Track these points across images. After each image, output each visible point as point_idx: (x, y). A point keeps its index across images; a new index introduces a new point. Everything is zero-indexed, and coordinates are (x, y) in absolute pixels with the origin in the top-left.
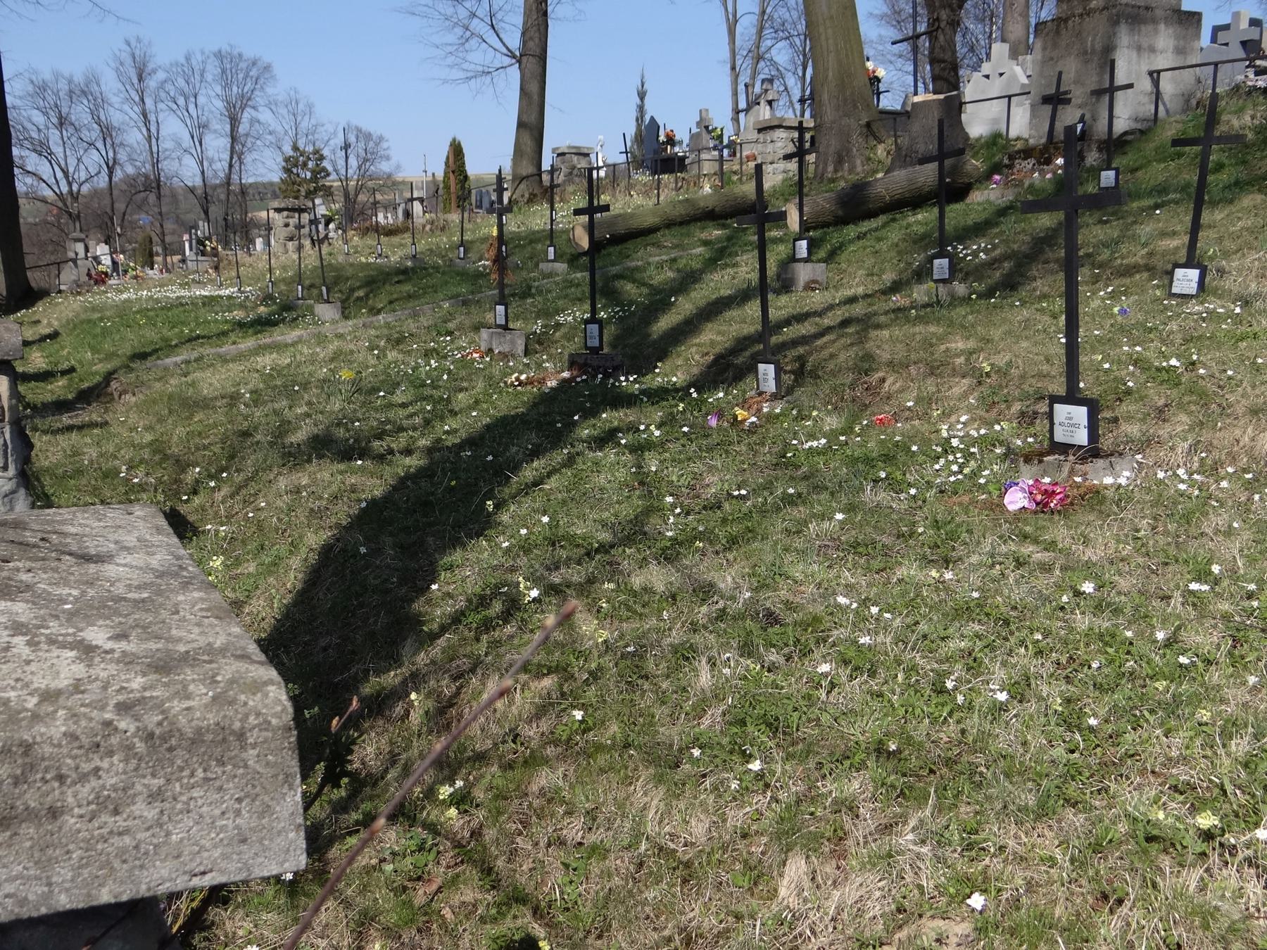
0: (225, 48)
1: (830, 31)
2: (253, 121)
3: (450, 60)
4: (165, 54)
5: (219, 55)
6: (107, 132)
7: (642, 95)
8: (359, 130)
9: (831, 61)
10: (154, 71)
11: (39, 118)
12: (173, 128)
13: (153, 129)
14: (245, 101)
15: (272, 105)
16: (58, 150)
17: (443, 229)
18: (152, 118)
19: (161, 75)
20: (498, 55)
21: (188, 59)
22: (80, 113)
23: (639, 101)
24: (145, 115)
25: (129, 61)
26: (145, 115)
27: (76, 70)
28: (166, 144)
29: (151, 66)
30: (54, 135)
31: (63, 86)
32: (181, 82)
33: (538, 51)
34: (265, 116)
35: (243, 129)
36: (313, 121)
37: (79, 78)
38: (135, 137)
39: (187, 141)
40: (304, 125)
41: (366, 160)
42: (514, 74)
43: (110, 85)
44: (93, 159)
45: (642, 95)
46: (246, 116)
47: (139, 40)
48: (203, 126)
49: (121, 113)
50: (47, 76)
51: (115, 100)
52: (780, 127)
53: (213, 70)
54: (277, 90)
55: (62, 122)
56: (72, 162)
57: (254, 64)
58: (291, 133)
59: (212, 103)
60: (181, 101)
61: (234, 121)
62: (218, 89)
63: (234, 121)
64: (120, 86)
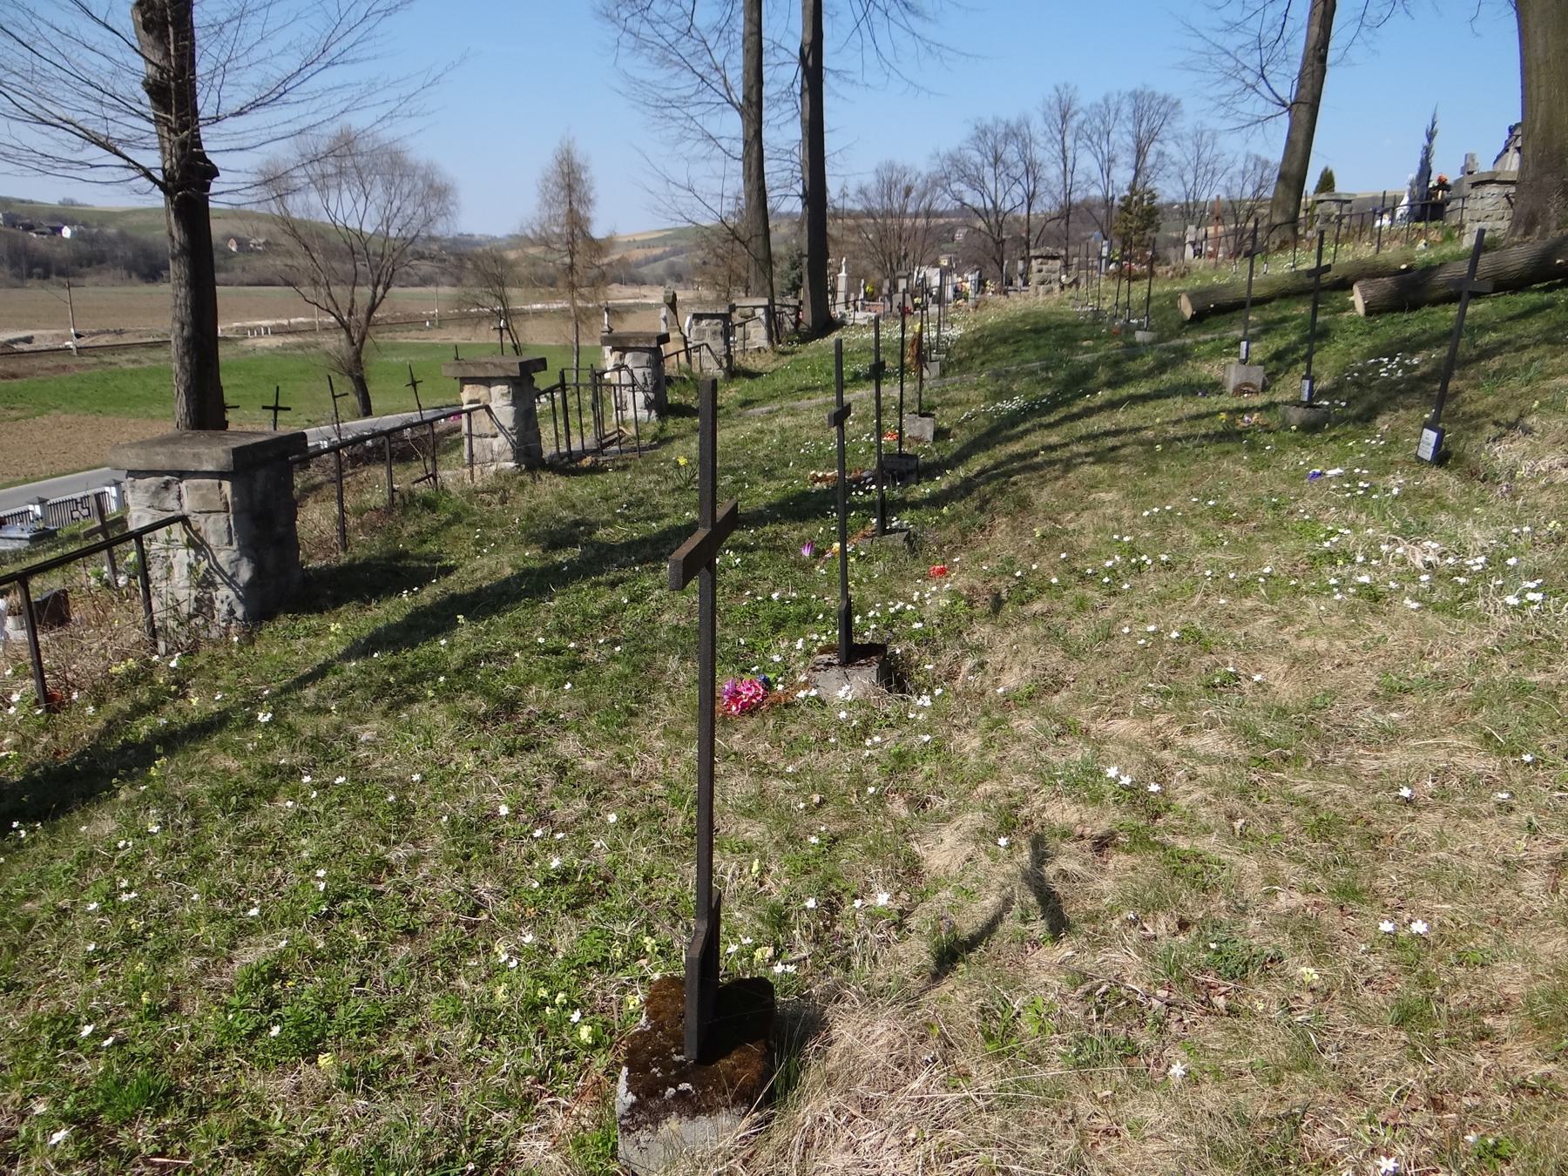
0: (1140, 88)
1: (1543, 78)
2: (1161, 154)
3: (1222, 111)
4: (1087, 97)
5: (1135, 96)
6: (1031, 169)
7: (1431, 136)
8: (1258, 158)
9: (1542, 108)
10: (1076, 113)
11: (978, 158)
12: (1087, 163)
13: (1070, 165)
14: (1152, 136)
15: (1177, 138)
16: (991, 186)
17: (1183, 276)
18: (1070, 154)
19: (1081, 116)
20: (1264, 102)
21: (1106, 100)
22: (1011, 153)
23: (1426, 142)
24: (1064, 151)
25: (1056, 107)
26: (1064, 151)
27: (1011, 114)
28: (1079, 177)
29: (1074, 109)
30: (988, 172)
31: (1001, 129)
32: (1097, 122)
33: (1309, 99)
34: (1171, 148)
35: (1150, 159)
36: (1216, 151)
37: (974, 133)
38: (1052, 172)
39: (1096, 173)
40: (1206, 156)
41: (1260, 187)
42: (1285, 121)
43: (1038, 127)
44: (1018, 191)
45: (1431, 136)
46: (1152, 151)
47: (1066, 86)
48: (1111, 160)
49: (1044, 153)
50: (990, 122)
51: (1042, 140)
52: (1491, 182)
53: (1127, 110)
54: (1184, 125)
55: (997, 159)
56: (1000, 195)
57: (1165, 100)
58: (1193, 164)
59: (1122, 139)
60: (1095, 138)
61: (1140, 153)
62: (1130, 126)
63: (1140, 153)
64: (1046, 127)
